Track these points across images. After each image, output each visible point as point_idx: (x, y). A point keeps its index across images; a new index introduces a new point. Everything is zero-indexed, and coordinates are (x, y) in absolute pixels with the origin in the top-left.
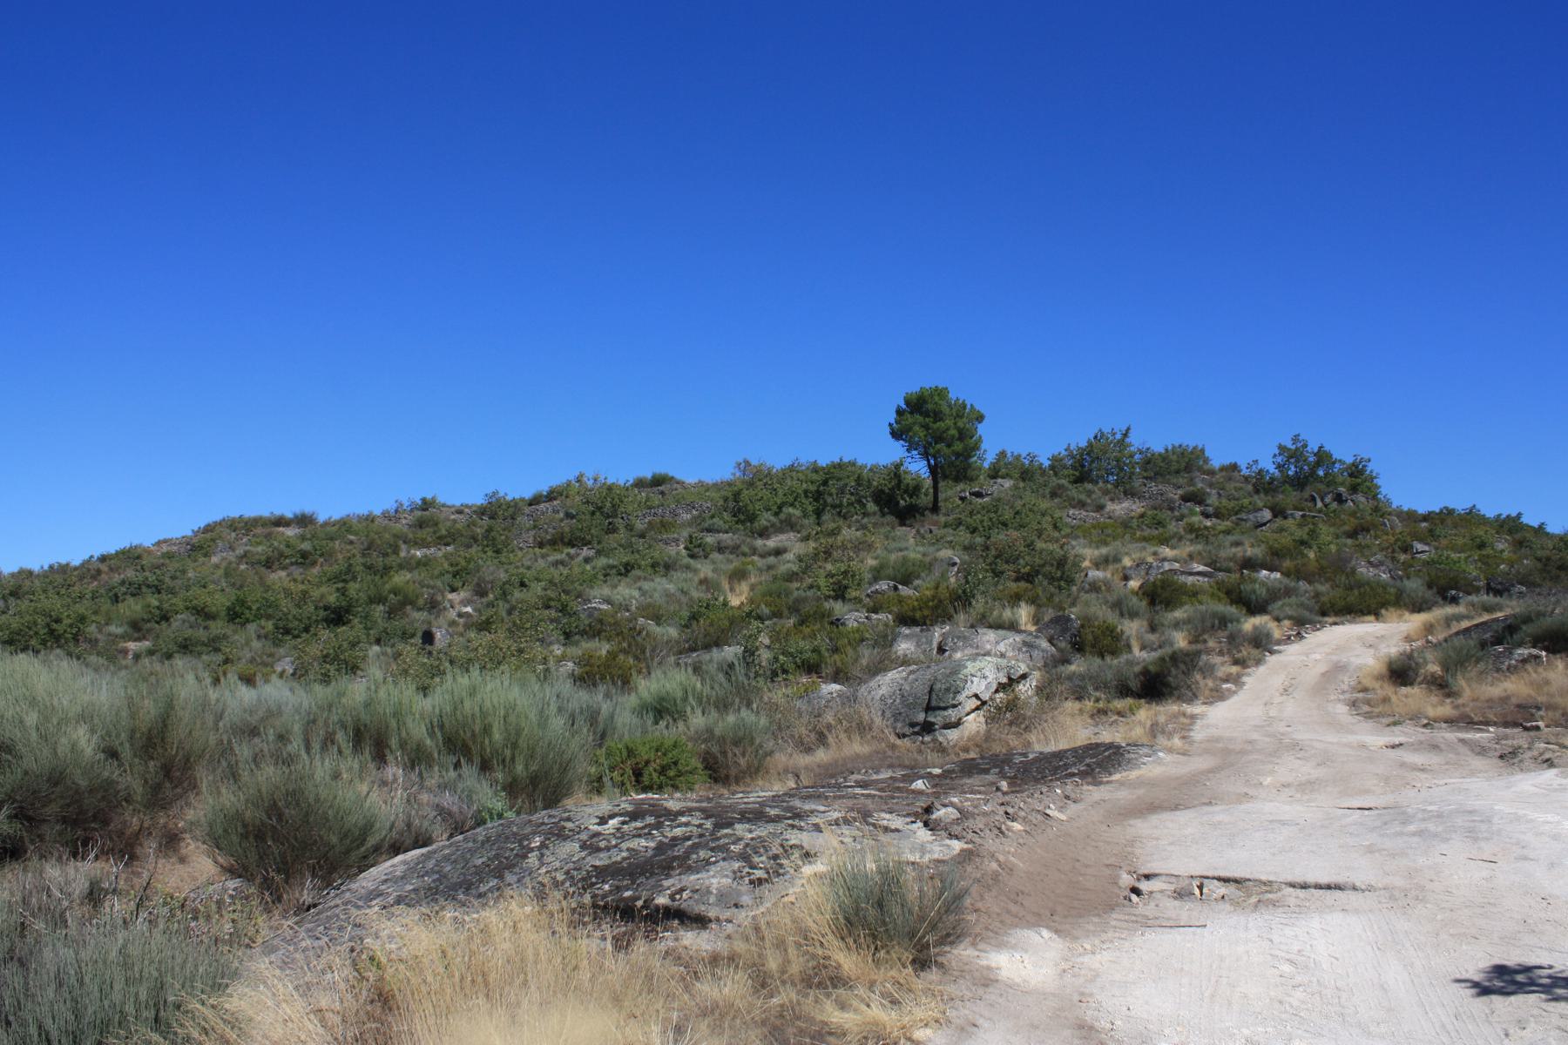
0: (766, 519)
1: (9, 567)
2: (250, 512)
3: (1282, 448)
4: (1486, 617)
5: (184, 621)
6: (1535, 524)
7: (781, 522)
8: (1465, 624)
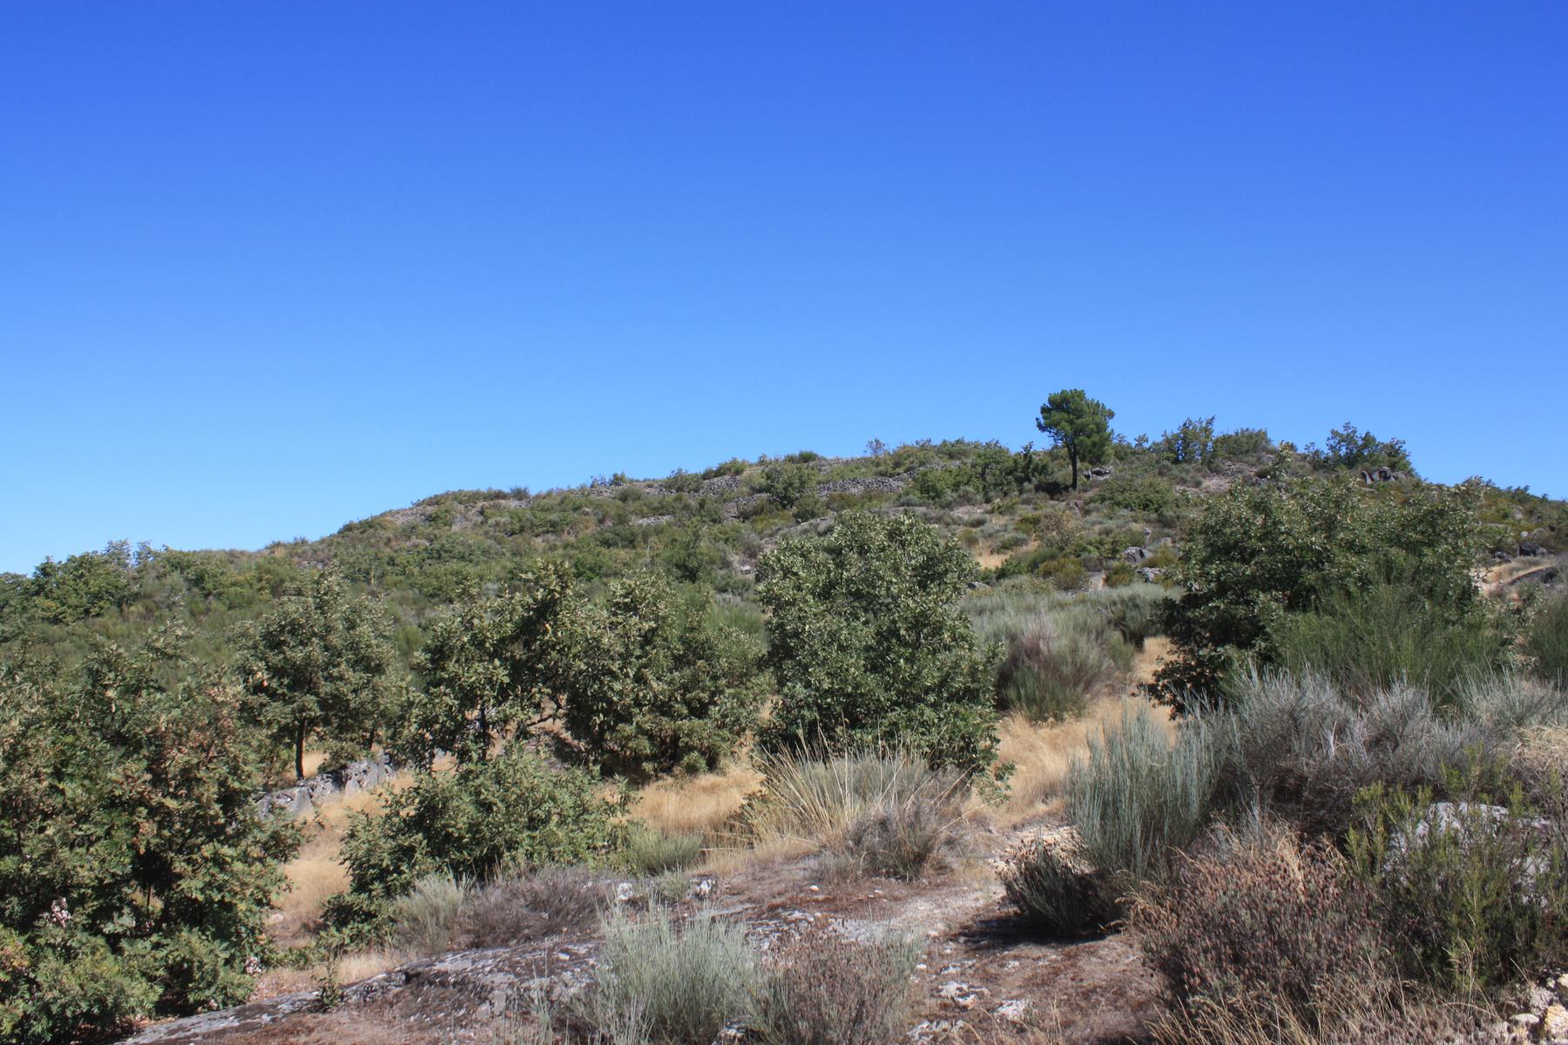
0: (949, 495)
2: (470, 486)
3: (1335, 433)
4: (1534, 569)
6: (1540, 495)
8: (1521, 573)
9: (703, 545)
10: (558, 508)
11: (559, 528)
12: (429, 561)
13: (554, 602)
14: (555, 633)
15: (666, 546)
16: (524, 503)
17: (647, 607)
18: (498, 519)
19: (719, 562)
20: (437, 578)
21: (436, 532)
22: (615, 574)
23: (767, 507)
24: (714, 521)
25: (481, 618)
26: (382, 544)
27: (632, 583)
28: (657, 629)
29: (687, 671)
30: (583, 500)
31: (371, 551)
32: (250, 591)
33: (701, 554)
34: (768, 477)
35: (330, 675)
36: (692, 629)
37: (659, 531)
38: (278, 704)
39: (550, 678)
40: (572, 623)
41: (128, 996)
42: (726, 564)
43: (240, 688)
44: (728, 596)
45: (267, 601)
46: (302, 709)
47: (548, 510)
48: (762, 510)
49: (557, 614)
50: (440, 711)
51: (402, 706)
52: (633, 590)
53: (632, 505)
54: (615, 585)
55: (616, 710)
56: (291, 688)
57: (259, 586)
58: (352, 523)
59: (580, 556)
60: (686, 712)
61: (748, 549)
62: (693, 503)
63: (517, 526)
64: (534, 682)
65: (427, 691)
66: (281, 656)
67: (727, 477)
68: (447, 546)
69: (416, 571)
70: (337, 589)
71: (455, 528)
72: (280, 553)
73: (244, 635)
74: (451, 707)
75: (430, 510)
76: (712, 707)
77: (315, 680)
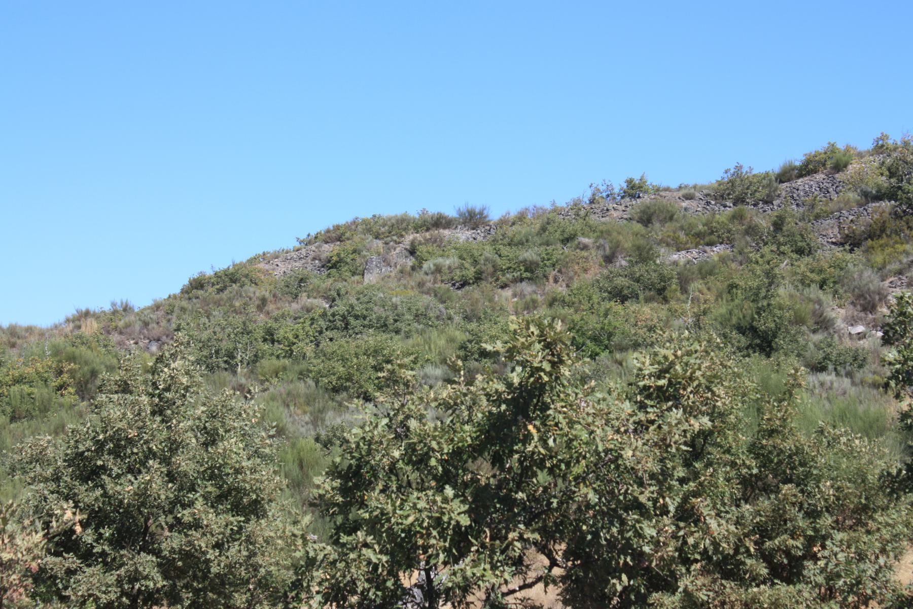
1: (5, 324)
2: (390, 209)
5: (643, 363)
9: (784, 292)
10: (538, 240)
11: (539, 272)
12: (329, 334)
13: (540, 388)
14: (544, 441)
15: (719, 296)
16: (480, 233)
17: (695, 392)
18: (440, 260)
19: (811, 322)
20: (344, 360)
21: (340, 285)
22: (636, 346)
23: (892, 225)
24: (800, 252)
25: (420, 419)
26: (252, 309)
27: (669, 353)
28: (711, 433)
29: (765, 503)
30: (578, 225)
31: (238, 320)
32: (45, 391)
33: (781, 308)
34: (892, 173)
35: (178, 521)
36: (771, 433)
37: (706, 272)
38: (97, 569)
39: (538, 516)
40: (571, 423)
41: (685, 269)
42: (823, 324)
43: (38, 537)
44: (828, 377)
45: (72, 406)
46: (134, 577)
47: (521, 243)
48: (883, 230)
49: (546, 407)
50: (358, 572)
51: (295, 567)
52: (672, 364)
53: (659, 230)
54: (638, 360)
55: (648, 569)
56: (117, 542)
57: (59, 381)
58: (202, 274)
59: (577, 317)
60: (764, 571)
61: (861, 296)
62: (764, 223)
63: (471, 272)
64: (510, 522)
65: (336, 542)
66: (99, 492)
67: (820, 177)
68: (359, 309)
69: (309, 350)
70: (185, 380)
71: (370, 278)
72: (90, 328)
73: (39, 459)
74: (376, 567)
75: (328, 250)
76: (809, 564)
77: (153, 528)
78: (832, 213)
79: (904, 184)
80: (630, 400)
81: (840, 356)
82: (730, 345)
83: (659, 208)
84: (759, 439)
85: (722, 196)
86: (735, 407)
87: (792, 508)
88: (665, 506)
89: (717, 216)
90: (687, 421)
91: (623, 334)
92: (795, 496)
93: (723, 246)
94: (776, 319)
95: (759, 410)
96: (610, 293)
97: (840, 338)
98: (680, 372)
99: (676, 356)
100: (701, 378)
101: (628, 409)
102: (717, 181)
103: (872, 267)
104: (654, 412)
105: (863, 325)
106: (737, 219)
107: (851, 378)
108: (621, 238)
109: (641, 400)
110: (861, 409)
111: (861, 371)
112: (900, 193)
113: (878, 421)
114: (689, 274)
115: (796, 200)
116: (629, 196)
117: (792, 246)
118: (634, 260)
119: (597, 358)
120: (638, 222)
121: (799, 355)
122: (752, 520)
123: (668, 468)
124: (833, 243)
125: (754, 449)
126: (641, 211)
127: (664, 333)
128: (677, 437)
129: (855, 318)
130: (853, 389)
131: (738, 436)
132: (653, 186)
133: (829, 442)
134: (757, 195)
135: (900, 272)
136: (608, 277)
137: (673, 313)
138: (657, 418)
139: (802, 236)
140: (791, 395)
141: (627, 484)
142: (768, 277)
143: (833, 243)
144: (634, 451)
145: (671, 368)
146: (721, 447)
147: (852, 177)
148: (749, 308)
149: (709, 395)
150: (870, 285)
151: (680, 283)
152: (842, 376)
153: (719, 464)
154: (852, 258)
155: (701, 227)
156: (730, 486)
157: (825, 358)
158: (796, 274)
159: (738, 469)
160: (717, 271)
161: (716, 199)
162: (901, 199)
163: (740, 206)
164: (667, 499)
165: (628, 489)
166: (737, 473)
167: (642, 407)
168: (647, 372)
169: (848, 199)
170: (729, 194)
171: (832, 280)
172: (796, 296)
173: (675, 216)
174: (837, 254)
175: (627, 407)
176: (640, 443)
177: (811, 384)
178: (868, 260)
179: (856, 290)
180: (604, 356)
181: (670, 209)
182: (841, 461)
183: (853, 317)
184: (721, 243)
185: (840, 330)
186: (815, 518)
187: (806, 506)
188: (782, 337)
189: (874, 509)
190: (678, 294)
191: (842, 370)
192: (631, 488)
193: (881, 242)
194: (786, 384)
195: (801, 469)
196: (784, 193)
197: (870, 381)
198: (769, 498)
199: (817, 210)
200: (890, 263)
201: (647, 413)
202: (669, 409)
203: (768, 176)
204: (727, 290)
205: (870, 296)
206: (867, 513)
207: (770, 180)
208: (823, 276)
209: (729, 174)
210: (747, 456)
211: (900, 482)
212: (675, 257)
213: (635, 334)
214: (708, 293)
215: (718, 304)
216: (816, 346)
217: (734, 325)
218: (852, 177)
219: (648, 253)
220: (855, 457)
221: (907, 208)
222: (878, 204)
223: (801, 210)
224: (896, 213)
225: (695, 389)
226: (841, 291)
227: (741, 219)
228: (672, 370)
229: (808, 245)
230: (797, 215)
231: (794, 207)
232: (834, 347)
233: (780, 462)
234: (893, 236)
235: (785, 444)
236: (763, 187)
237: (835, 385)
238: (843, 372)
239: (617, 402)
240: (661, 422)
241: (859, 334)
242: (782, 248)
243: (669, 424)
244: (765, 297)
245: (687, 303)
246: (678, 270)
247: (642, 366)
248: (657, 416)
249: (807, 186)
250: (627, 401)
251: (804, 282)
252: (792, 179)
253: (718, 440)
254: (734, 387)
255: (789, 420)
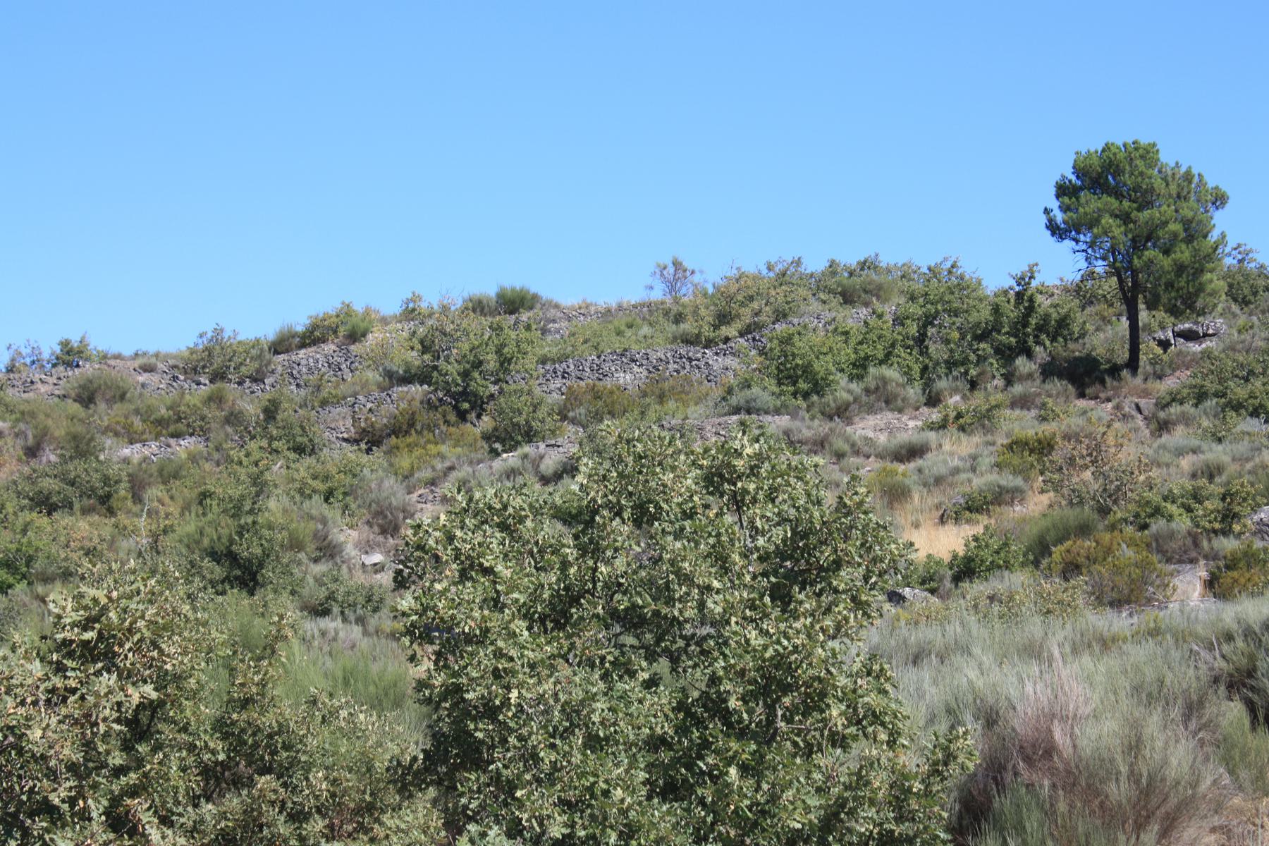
0: (844, 389)
5: (64, 608)
7: (867, 391)
9: (275, 506)
15: (186, 508)
17: (137, 649)
19: (311, 547)
23: (424, 417)
24: (300, 450)
27: (101, 595)
28: (161, 703)
29: (234, 802)
36: (246, 703)
37: (169, 474)
41: (140, 469)
42: (328, 550)
48: (411, 424)
52: (104, 610)
53: (104, 413)
54: (60, 599)
61: (380, 513)
62: (251, 408)
67: (329, 348)
78: (344, 398)
79: (441, 363)
80: (42, 660)
81: (349, 596)
82: (197, 579)
83: (105, 383)
84: (228, 713)
85: (195, 369)
86: (196, 667)
87: (271, 809)
88: (86, 809)
89: (188, 397)
90: (122, 690)
91: (48, 558)
92: (275, 791)
93: (194, 438)
94: (263, 542)
95: (232, 670)
96: (31, 499)
97: (350, 570)
98: (116, 621)
99: (110, 599)
100: (144, 631)
101: (37, 672)
102: (188, 348)
103: (396, 474)
104: (77, 677)
105: (381, 553)
106: (215, 402)
107: (363, 625)
108: (50, 422)
109: (58, 661)
110: (375, 668)
111: (376, 616)
112: (435, 374)
113: (395, 685)
114: (145, 476)
115: (296, 379)
116: (64, 363)
117: (288, 441)
118: (68, 455)
119: (9, 591)
120: (75, 400)
121: (293, 593)
122: (215, 826)
123: (100, 753)
124: (345, 440)
125: (221, 727)
126: (80, 386)
127: (94, 566)
128: (107, 712)
129: (371, 543)
130: (366, 639)
131: (199, 708)
132: (98, 352)
133: (323, 717)
134: (243, 369)
135: (433, 483)
136: (29, 478)
137: (121, 530)
138: (79, 686)
139: (303, 428)
140: (273, 652)
141: (33, 779)
142: (254, 484)
143: (345, 440)
144: (44, 729)
145: (103, 615)
146: (176, 723)
147: (372, 351)
148: (228, 526)
149: (155, 653)
150: (393, 499)
151: (132, 488)
152: (351, 623)
153: (172, 747)
154: (369, 461)
155: (163, 411)
156: (186, 778)
157: (328, 598)
158: (294, 480)
159: (198, 754)
160: (184, 473)
161: (186, 373)
162: (437, 383)
163: (219, 385)
164: (90, 801)
165: (35, 786)
166: (195, 761)
167: (60, 669)
168: (68, 620)
169: (367, 380)
170: (204, 367)
171: (342, 490)
172: (292, 511)
173: (128, 395)
174: (349, 454)
175: (37, 668)
176: (54, 720)
177: (309, 634)
178: (391, 465)
179: (374, 505)
180: (20, 588)
181: (121, 384)
182: (339, 742)
183: (368, 541)
184: (191, 435)
185: (350, 559)
186: (301, 823)
187: (290, 805)
188: (270, 567)
189: (381, 808)
190: (129, 503)
191: (351, 614)
192: (39, 785)
193: (409, 440)
194: (266, 637)
195: (285, 754)
196: (280, 369)
197: (388, 630)
198: (240, 795)
199: (324, 394)
200: (419, 469)
201: (66, 677)
202: (98, 673)
203: (258, 344)
204: (197, 501)
205: (391, 513)
206: (372, 815)
207: (262, 350)
208: (329, 484)
209: (205, 339)
210: (212, 736)
211: (416, 775)
212: (126, 452)
213: (66, 559)
214: (171, 503)
215: (183, 520)
216: (316, 580)
217: (205, 550)
218: (372, 351)
219: (88, 444)
220: (358, 738)
221: (445, 395)
222: (405, 389)
223: (303, 392)
224: (429, 401)
225: (135, 645)
226: (353, 506)
227: (220, 401)
228: (103, 618)
229: (311, 440)
230: (297, 399)
231: (293, 387)
232: (342, 583)
233: (256, 745)
234: (425, 432)
235: (264, 719)
236: (252, 358)
237: (342, 634)
238: (352, 618)
239: (22, 662)
240: (84, 691)
241: (375, 565)
242: (275, 444)
243: (97, 694)
244: (251, 512)
245: (141, 516)
246: (130, 471)
247: (61, 612)
248: (81, 682)
249: (311, 360)
250: (38, 660)
251: (304, 492)
252: (292, 350)
253: (171, 714)
254: (197, 640)
255: (270, 685)
